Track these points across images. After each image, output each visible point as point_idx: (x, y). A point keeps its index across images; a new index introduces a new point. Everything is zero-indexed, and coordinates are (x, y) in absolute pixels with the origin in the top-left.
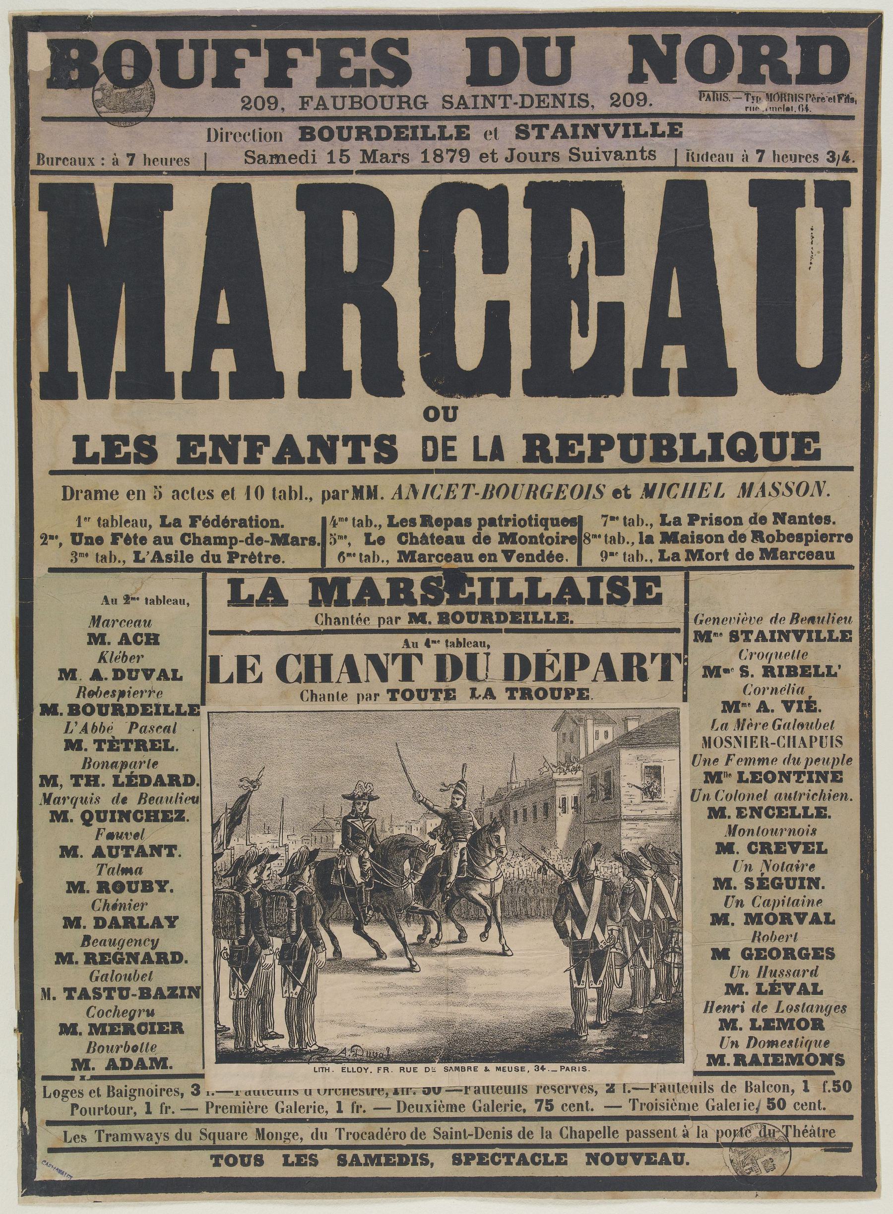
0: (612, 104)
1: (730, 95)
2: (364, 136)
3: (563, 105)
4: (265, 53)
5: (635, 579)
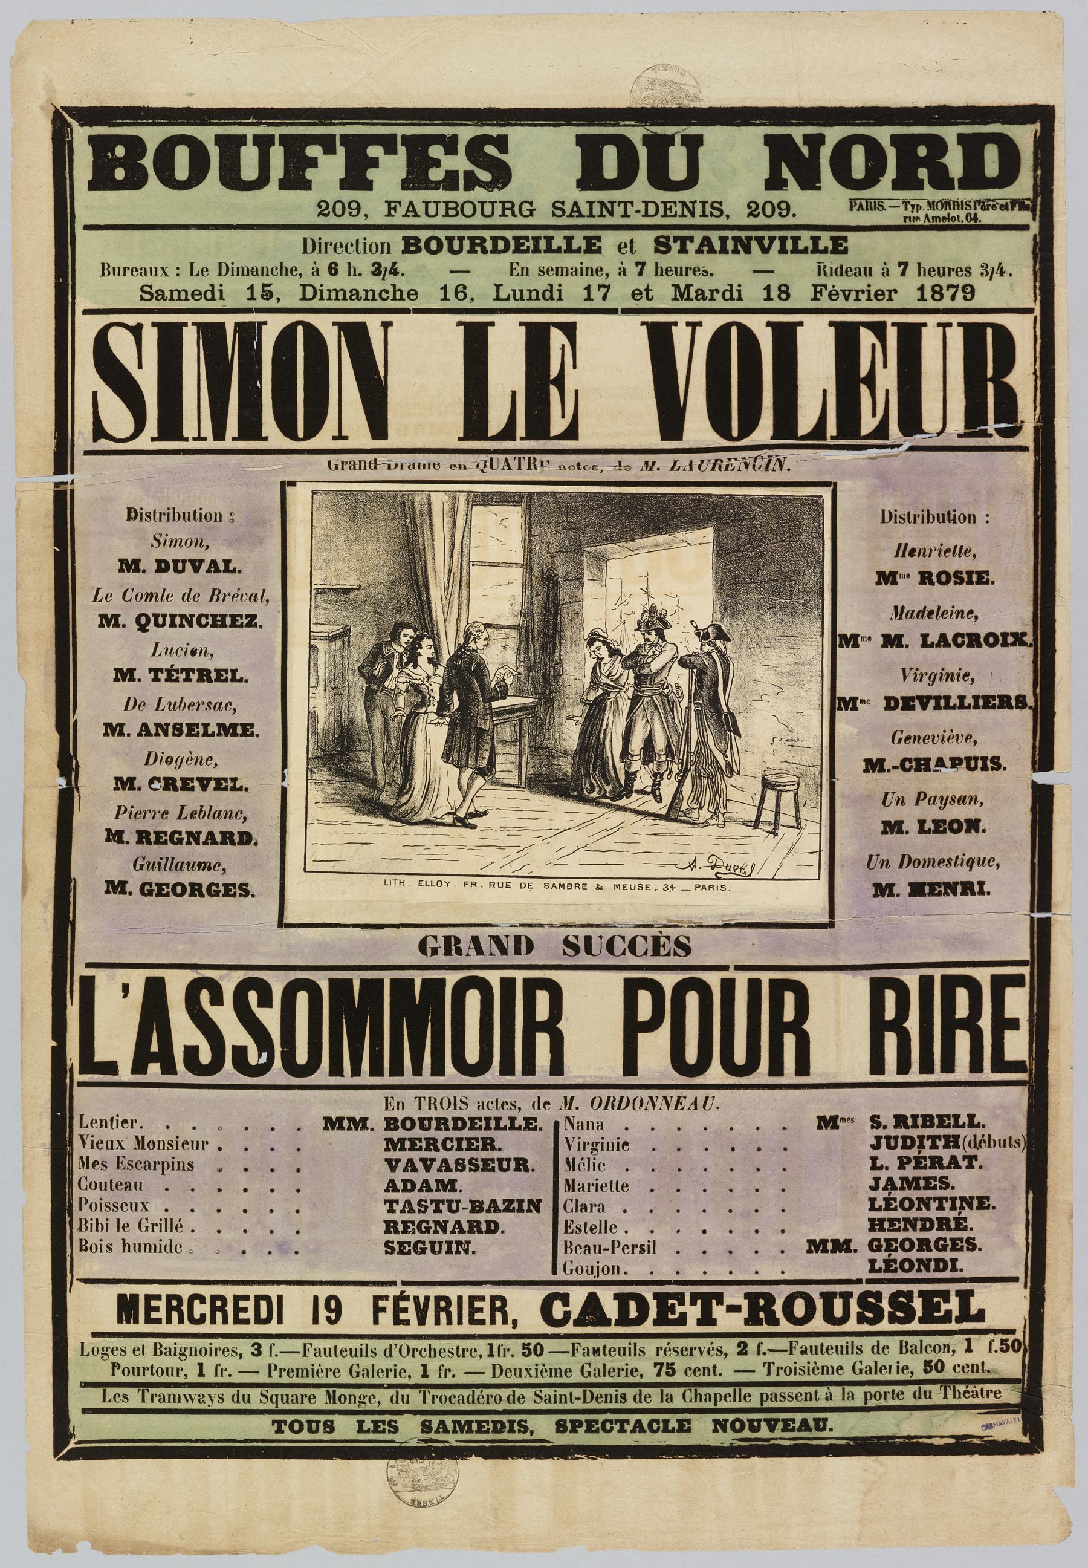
0: (750, 214)
1: (886, 204)
2: (478, 249)
3: (693, 214)
4: (341, 150)
5: (921, 1294)
